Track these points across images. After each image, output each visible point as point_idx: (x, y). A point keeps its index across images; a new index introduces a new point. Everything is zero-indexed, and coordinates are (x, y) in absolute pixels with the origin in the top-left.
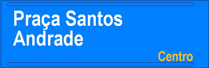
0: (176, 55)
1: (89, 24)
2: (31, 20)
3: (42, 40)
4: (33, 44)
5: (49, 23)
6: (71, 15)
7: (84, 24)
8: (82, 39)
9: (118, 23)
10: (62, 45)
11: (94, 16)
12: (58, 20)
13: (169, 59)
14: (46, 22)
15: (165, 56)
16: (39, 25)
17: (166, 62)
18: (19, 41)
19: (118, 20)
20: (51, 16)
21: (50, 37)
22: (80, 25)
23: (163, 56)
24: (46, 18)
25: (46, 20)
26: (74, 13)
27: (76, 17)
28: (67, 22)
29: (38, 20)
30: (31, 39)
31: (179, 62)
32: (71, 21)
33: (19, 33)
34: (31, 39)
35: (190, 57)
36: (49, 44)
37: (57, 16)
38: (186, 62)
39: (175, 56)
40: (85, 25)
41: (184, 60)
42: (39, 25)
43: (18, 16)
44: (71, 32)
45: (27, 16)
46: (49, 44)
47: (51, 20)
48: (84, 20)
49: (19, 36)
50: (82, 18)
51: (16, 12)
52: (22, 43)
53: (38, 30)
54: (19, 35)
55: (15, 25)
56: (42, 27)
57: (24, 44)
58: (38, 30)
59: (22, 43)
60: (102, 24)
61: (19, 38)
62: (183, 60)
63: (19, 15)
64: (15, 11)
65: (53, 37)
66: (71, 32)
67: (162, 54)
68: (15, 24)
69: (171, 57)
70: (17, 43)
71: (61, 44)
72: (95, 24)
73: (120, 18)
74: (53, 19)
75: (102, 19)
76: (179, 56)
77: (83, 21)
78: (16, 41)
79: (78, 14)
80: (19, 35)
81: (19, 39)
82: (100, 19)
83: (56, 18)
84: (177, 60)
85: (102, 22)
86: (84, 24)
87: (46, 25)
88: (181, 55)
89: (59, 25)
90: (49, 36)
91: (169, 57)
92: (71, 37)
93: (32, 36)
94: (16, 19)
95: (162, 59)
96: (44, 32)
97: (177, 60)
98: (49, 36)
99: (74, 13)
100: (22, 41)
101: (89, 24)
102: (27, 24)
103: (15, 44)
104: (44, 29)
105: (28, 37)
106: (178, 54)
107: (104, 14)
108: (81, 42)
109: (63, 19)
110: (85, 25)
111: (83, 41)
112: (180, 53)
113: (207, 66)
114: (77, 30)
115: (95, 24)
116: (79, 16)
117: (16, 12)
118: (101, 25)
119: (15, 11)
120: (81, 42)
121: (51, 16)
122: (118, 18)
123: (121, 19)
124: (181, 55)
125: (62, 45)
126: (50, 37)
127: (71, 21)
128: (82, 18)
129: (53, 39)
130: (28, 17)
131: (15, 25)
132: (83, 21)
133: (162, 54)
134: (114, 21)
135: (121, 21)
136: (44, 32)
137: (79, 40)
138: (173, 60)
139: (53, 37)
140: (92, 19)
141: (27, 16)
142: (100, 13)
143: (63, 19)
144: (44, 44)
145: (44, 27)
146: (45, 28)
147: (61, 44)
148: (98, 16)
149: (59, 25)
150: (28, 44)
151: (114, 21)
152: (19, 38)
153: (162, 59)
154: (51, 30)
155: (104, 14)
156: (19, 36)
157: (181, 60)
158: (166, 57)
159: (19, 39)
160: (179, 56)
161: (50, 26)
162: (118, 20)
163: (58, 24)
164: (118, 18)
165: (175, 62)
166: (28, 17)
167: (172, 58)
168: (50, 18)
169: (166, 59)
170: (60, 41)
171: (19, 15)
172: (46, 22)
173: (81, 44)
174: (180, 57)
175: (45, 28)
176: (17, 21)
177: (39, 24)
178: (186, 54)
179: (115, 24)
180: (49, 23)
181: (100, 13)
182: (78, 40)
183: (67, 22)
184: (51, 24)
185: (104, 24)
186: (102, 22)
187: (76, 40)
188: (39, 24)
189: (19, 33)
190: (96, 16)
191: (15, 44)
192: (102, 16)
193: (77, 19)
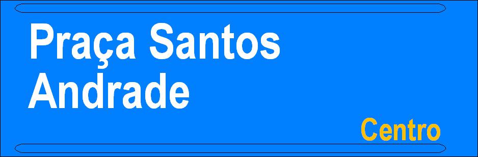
0: (402, 126)
1: (203, 55)
2: (68, 45)
3: (98, 94)
4: (75, 105)
5: (110, 53)
6: (162, 33)
7: (191, 54)
8: (186, 93)
9: (270, 51)
10: (139, 106)
11: (213, 36)
12: (131, 44)
13: (386, 135)
14: (103, 51)
15: (376, 129)
16: (88, 57)
17: (378, 142)
18: (43, 98)
19: (270, 45)
20: (115, 36)
21: (112, 87)
22: (181, 56)
23: (371, 129)
24: (103, 41)
25: (104, 46)
26: (169, 30)
27: (173, 38)
28: (153, 50)
29: (85, 46)
30: (69, 92)
31: (408, 143)
32: (162, 48)
33: (43, 78)
34: (69, 92)
35: (434, 132)
36: (111, 105)
37: (130, 36)
38: (426, 142)
39: (400, 131)
40: (193, 57)
41: (420, 138)
42: (88, 57)
43: (41, 35)
44: (163, 76)
45: (59, 35)
46: (111, 105)
47: (114, 45)
48: (191, 45)
49: (43, 85)
50: (186, 40)
51: (35, 27)
52: (48, 101)
53: (84, 71)
54: (43, 84)
55: (165, 74)
56: (95, 60)
57: (53, 105)
58: (84, 71)
59: (48, 101)
60: (233, 54)
61: (43, 91)
62: (417, 138)
63: (42, 34)
64: (33, 25)
65: (120, 88)
66: (163, 76)
67: (369, 124)
68: (34, 55)
69: (390, 131)
70: (38, 102)
71: (138, 104)
72: (216, 55)
73: (274, 40)
74: (120, 42)
75: (233, 42)
76: (407, 130)
77: (188, 47)
78: (36, 97)
79: (177, 32)
80: (43, 84)
81: (42, 92)
82: (227, 43)
83: (126, 40)
84: (404, 138)
85: (233, 49)
86: (191, 54)
87: (104, 57)
88: (414, 126)
89: (133, 57)
90: (110, 85)
91: (387, 133)
92: (99, 88)
93: (73, 86)
94: (35, 42)
95: (369, 135)
96: (100, 76)
97: (404, 138)
98: (110, 85)
99: (169, 30)
100: (49, 97)
101: (203, 55)
102: (60, 55)
103: (32, 105)
104: (100, 67)
105: (62, 87)
106: (406, 124)
107: (237, 32)
108: (183, 101)
109: (144, 42)
110: (193, 57)
111: (188, 96)
112: (411, 122)
113: (1, 1)
114: (176, 69)
115: (216, 55)
116: (181, 37)
117: (35, 27)
118: (229, 56)
119: (33, 25)
120: (183, 101)
121: (115, 36)
122: (270, 40)
123: (276, 42)
124: (414, 126)
125: (139, 106)
126: (112, 87)
127: (162, 48)
128: (186, 40)
129: (119, 94)
130: (62, 38)
131: (165, 74)
132: (188, 47)
133: (369, 124)
134: (261, 47)
135: (276, 49)
136: (100, 76)
137: (180, 95)
138: (396, 138)
139: (120, 88)
140: (209, 42)
141: (59, 35)
142: (227, 29)
143: (144, 42)
144: (99, 103)
145: (100, 61)
146: (102, 63)
147: (138, 104)
148: (223, 36)
149: (133, 57)
150: (62, 105)
151: (261, 47)
152: (43, 91)
153: (369, 135)
154: (119, 71)
155: (237, 32)
156: (43, 85)
157: (412, 139)
158: (378, 133)
159: (42, 92)
160: (407, 130)
161: (113, 59)
162: (270, 45)
163: (131, 54)
164: (270, 40)
165: (400, 143)
166: (62, 38)
167: (392, 134)
168: (376, 124)
169: (378, 137)
170: (135, 97)
171: (42, 34)
172: (103, 51)
173: (185, 104)
174: (409, 131)
175: (102, 63)
176: (38, 47)
177: (87, 55)
178: (424, 126)
179: (264, 54)
180: (110, 53)
181: (227, 29)
182: (178, 96)
183: (153, 50)
184: (114, 54)
185: (237, 55)
186: (233, 49)
187: (173, 95)
188: (87, 55)
189: (43, 78)
190: (220, 36)
191: (32, 105)
192: (232, 36)
193: (176, 43)
